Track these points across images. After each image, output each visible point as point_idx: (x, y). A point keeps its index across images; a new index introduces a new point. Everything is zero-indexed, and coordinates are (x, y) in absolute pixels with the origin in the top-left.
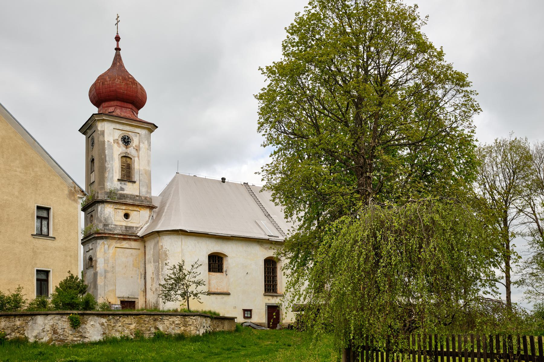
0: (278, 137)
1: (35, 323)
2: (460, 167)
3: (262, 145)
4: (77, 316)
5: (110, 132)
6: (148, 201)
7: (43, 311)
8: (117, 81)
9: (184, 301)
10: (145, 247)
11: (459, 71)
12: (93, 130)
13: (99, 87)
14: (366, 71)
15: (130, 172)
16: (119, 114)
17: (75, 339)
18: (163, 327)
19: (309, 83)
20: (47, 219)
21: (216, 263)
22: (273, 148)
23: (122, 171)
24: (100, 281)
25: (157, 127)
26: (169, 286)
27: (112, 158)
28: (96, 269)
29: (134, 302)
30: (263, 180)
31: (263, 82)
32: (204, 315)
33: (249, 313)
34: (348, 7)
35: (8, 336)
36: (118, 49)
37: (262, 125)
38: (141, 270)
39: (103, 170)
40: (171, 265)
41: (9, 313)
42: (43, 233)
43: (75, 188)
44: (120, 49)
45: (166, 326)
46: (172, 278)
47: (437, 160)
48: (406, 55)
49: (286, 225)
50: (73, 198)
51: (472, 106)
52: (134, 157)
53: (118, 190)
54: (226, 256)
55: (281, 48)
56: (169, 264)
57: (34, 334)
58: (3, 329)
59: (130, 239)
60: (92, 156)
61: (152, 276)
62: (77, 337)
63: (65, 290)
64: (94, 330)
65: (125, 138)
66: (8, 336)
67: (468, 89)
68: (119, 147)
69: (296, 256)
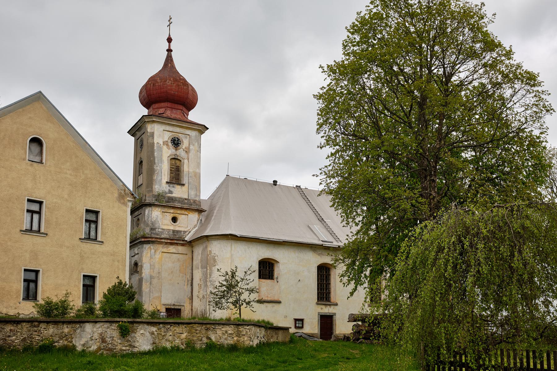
0: (336, 139)
1: (84, 331)
2: (529, 170)
3: (318, 147)
4: (127, 324)
5: (160, 134)
6: (197, 205)
7: (91, 318)
8: (169, 83)
9: (236, 309)
10: (193, 252)
11: (530, 70)
12: (142, 132)
13: (150, 89)
14: (430, 71)
15: (179, 175)
16: (169, 115)
17: (124, 348)
18: (216, 337)
19: (370, 83)
20: (96, 222)
21: (267, 269)
22: (329, 150)
23: (171, 173)
24: (145, 288)
25: (208, 129)
26: (220, 294)
27: (161, 161)
28: (141, 275)
29: (179, 310)
30: (321, 184)
31: (323, 81)
32: (258, 324)
33: (301, 322)
34: (412, 6)
35: (56, 344)
36: (169, 50)
37: (321, 125)
38: (188, 277)
39: (151, 172)
40: (223, 271)
41: (58, 319)
42: (91, 237)
43: (125, 191)
44: (171, 51)
45: (220, 336)
46: (224, 285)
47: (504, 162)
48: (472, 55)
49: (343, 231)
50: (122, 201)
51: (544, 107)
52: (184, 159)
53: (166, 193)
54: (277, 262)
55: (341, 47)
56: (221, 271)
57: (82, 343)
58: (51, 336)
59: (177, 244)
60: (141, 158)
61: (199, 282)
62: (126, 346)
63: (113, 297)
64: (143, 339)
65: (175, 140)
66: (56, 344)
67: (540, 89)
68: (169, 149)
69: (354, 263)
